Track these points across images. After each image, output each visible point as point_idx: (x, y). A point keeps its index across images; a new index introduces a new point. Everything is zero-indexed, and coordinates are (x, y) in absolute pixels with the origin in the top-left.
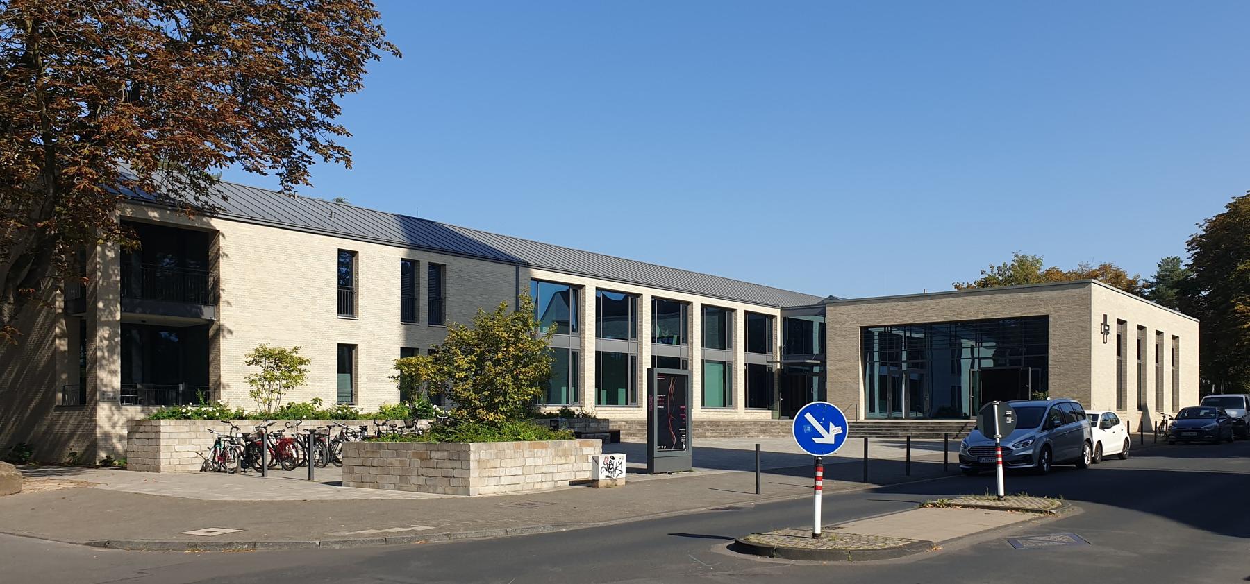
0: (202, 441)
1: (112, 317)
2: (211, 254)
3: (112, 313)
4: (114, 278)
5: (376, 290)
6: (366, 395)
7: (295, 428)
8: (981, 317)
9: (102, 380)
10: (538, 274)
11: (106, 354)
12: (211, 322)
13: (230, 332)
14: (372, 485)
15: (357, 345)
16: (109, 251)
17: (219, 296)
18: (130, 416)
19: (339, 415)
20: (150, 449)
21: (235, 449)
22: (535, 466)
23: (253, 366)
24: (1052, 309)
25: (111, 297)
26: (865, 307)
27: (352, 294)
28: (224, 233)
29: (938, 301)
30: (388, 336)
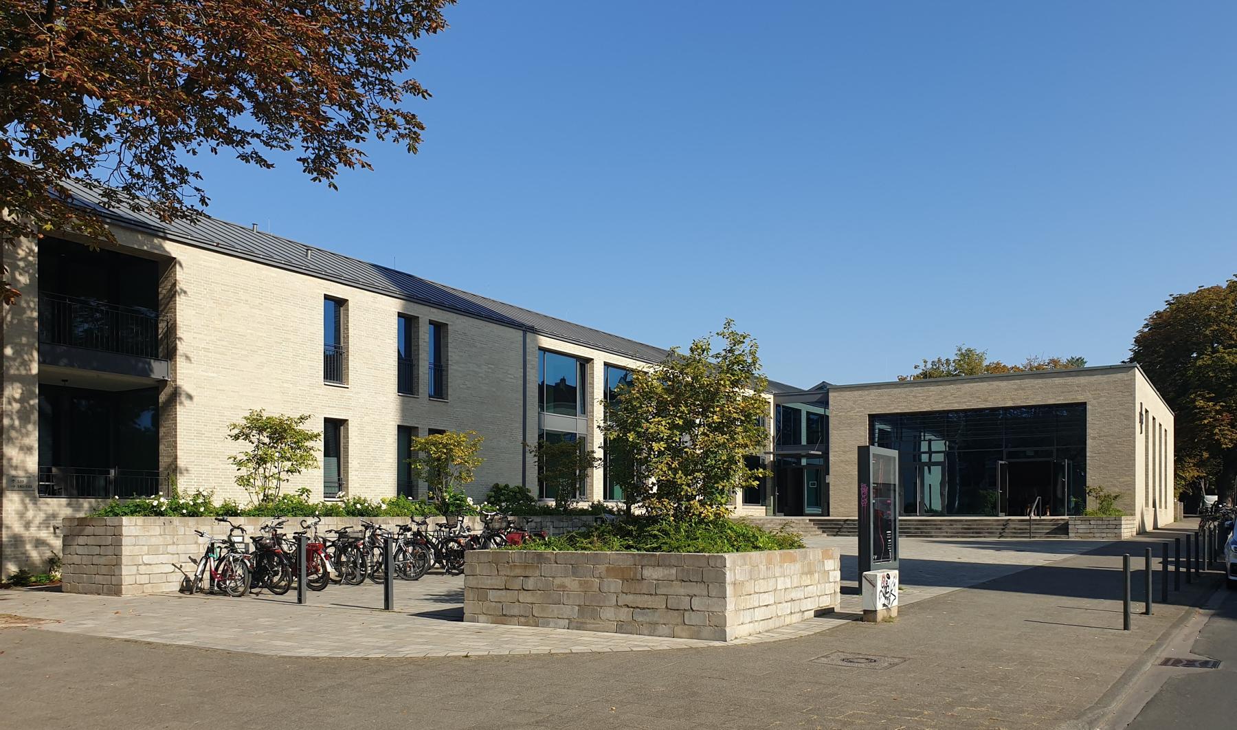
0: (181, 548)
1: (25, 369)
2: (163, 291)
3: (25, 364)
4: (29, 313)
5: (370, 351)
6: (357, 485)
7: (313, 528)
8: (1010, 404)
9: (10, 459)
10: (547, 342)
11: (17, 423)
12: (163, 383)
13: (190, 397)
14: (522, 619)
15: (347, 420)
16: (20, 274)
17: (175, 349)
18: (51, 512)
19: (359, 510)
20: (103, 560)
21: (242, 561)
22: (786, 589)
23: (240, 441)
24: (1090, 396)
25: (24, 340)
26: (874, 392)
27: (341, 354)
28: (182, 262)
29: (959, 386)
30: (384, 410)
